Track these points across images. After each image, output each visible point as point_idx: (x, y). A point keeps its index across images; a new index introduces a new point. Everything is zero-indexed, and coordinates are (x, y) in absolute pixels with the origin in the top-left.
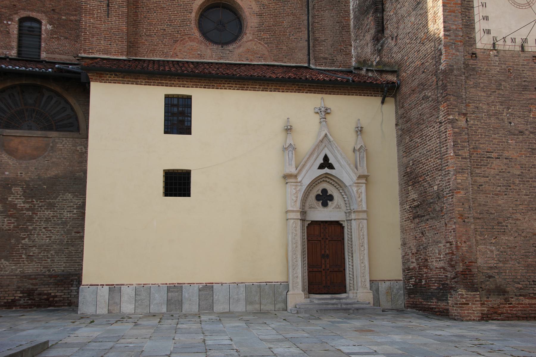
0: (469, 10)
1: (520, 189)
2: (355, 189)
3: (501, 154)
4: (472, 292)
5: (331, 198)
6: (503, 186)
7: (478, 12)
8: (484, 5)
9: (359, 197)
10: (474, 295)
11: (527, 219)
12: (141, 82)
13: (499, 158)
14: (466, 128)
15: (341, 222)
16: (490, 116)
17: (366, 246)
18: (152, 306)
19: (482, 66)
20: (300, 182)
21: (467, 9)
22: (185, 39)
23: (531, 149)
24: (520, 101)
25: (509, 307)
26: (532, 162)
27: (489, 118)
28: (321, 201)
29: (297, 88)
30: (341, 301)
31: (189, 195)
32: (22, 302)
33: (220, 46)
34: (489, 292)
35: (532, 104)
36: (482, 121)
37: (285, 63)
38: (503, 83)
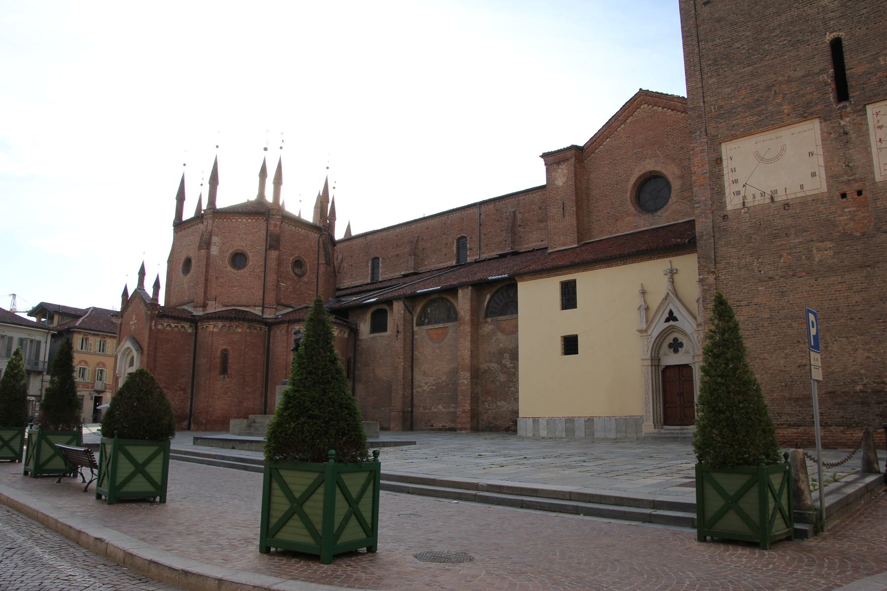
3: (750, 301)
6: (751, 330)
7: (728, 178)
8: (733, 170)
11: (774, 357)
12: (545, 276)
13: (749, 305)
14: (714, 284)
15: (690, 365)
16: (740, 269)
18: (557, 433)
19: (732, 225)
20: (650, 335)
21: (718, 178)
23: (780, 292)
24: (770, 249)
26: (782, 304)
27: (740, 270)
28: (673, 349)
29: (649, 257)
30: (683, 431)
31: (578, 354)
32: (512, 428)
33: (651, 214)
35: (782, 250)
36: (733, 274)
38: (754, 236)
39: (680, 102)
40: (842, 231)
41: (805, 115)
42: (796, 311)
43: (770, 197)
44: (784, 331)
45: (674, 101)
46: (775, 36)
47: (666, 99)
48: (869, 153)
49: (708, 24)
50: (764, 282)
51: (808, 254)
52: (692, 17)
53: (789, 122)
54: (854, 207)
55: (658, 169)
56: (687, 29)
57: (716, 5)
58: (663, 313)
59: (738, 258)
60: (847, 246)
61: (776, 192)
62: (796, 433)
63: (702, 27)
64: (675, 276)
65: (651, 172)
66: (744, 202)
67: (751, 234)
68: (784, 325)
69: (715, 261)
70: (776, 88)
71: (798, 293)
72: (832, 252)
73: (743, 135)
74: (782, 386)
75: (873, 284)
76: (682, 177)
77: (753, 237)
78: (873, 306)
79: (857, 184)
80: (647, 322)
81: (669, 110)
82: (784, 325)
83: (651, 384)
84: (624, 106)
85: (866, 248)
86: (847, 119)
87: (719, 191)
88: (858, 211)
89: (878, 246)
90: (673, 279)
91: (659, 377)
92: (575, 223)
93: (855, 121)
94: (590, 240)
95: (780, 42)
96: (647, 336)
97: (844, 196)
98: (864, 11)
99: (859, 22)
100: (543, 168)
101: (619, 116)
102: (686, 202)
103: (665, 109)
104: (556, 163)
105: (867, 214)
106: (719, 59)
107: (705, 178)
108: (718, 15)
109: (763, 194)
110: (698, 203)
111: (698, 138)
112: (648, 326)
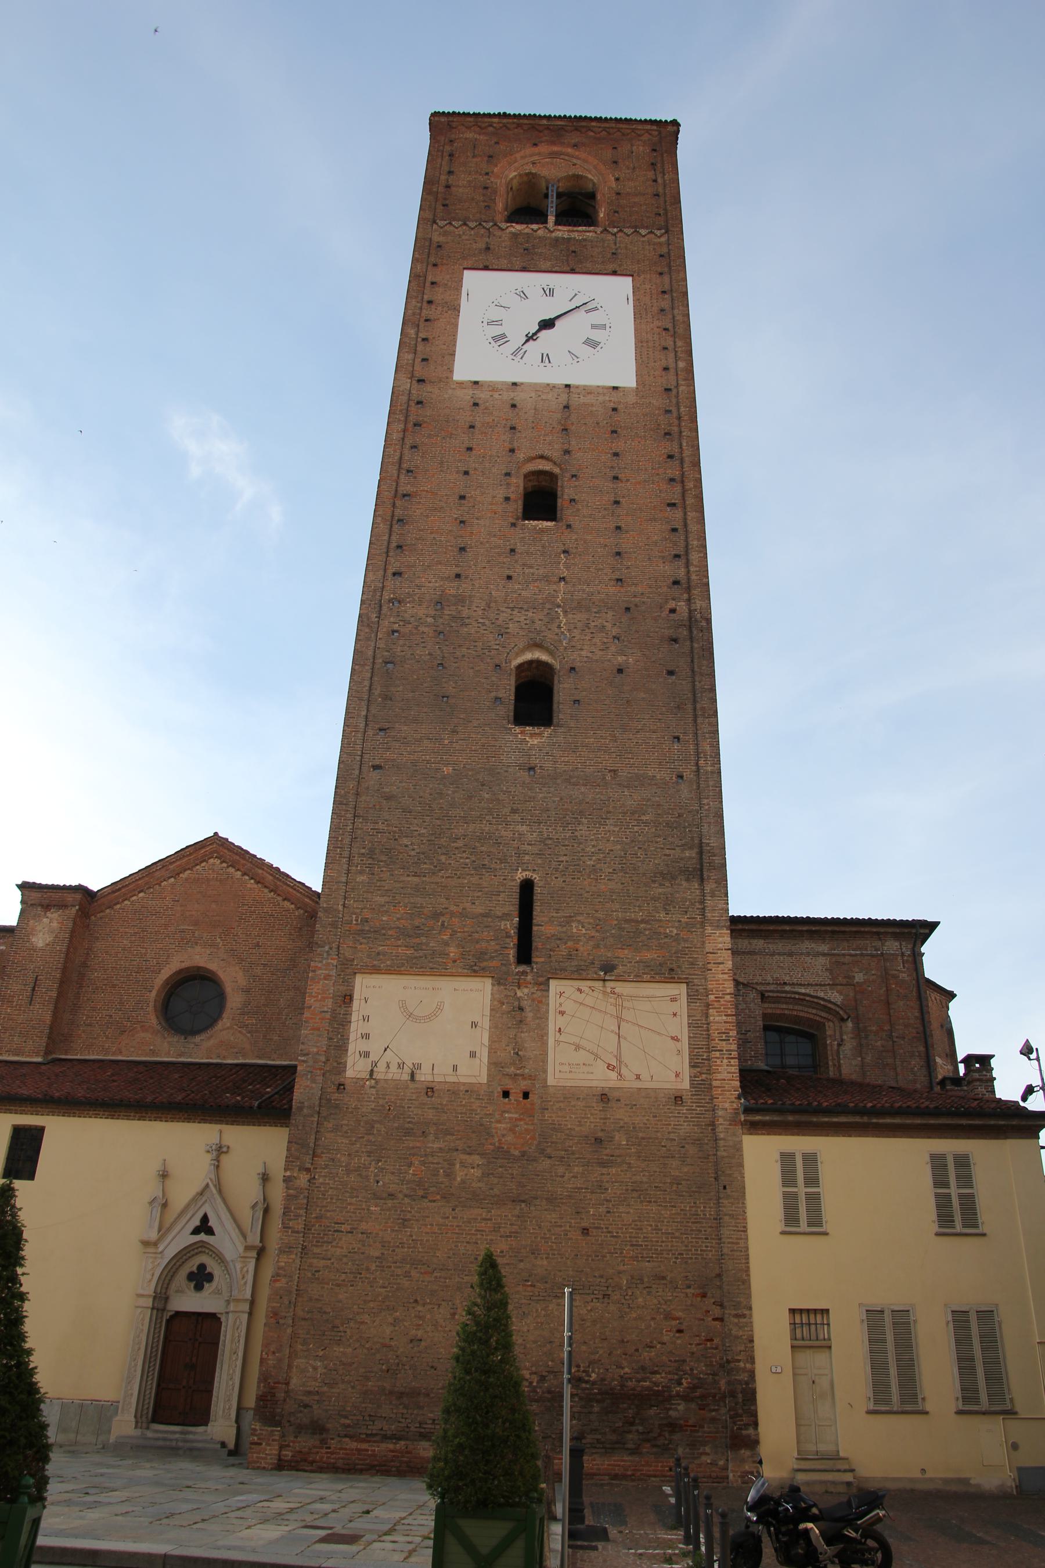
0: (343, 1025)
1: (375, 1278)
2: (239, 1266)
3: (356, 1226)
4: (270, 1426)
5: (210, 1277)
6: (350, 1273)
7: (356, 1028)
8: (366, 1019)
9: (243, 1278)
10: (272, 1431)
13: (352, 1233)
15: (219, 1316)
16: (348, 1172)
17: (241, 1354)
20: (161, 1252)
22: (136, 1028)
25: (327, 1453)
27: (348, 1175)
29: (186, 1116)
30: (187, 1436)
33: (183, 1037)
34: (300, 1429)
36: (337, 1179)
37: (274, 1060)
39: (271, 875)
40: (497, 1144)
41: (475, 968)
42: (419, 1252)
43: (410, 1072)
44: (398, 1281)
45: (263, 869)
46: (457, 848)
47: (251, 862)
48: (545, 1044)
49: (373, 796)
50: (381, 1199)
51: (449, 1168)
52: (353, 779)
53: (454, 971)
54: (516, 1113)
55: (213, 966)
56: (343, 792)
57: (389, 776)
58: (193, 1215)
59: (349, 1155)
60: (500, 1167)
61: (419, 1066)
62: (393, 1451)
63: (364, 798)
64: (224, 1158)
65: (199, 968)
66: (372, 1071)
67: (373, 1120)
68: (399, 1271)
69: (314, 1153)
70: (444, 918)
71: (426, 1225)
72: (480, 1171)
73: (389, 971)
74: (382, 1370)
75: (525, 1229)
76: (247, 991)
77: (376, 1126)
78: (521, 1261)
79: (525, 1083)
80: (159, 1231)
81: (252, 881)
82: (399, 1271)
83: (144, 1343)
84: (182, 850)
85: (523, 1175)
86: (526, 991)
87: (339, 1046)
88: (521, 1120)
89: (538, 1175)
90: (218, 1161)
91: (160, 1332)
92: (48, 1018)
93: (535, 996)
94: (66, 1055)
95: (461, 858)
96: (156, 1253)
97: (506, 1094)
98: (564, 858)
99: (557, 870)
100: (18, 907)
101: (171, 863)
102: (244, 1032)
103: (247, 878)
104: (42, 906)
105: (531, 1127)
106: (377, 851)
107: (323, 1019)
108: (388, 790)
109: (401, 1066)
110: (305, 1055)
111: (325, 955)
112: (162, 1236)
